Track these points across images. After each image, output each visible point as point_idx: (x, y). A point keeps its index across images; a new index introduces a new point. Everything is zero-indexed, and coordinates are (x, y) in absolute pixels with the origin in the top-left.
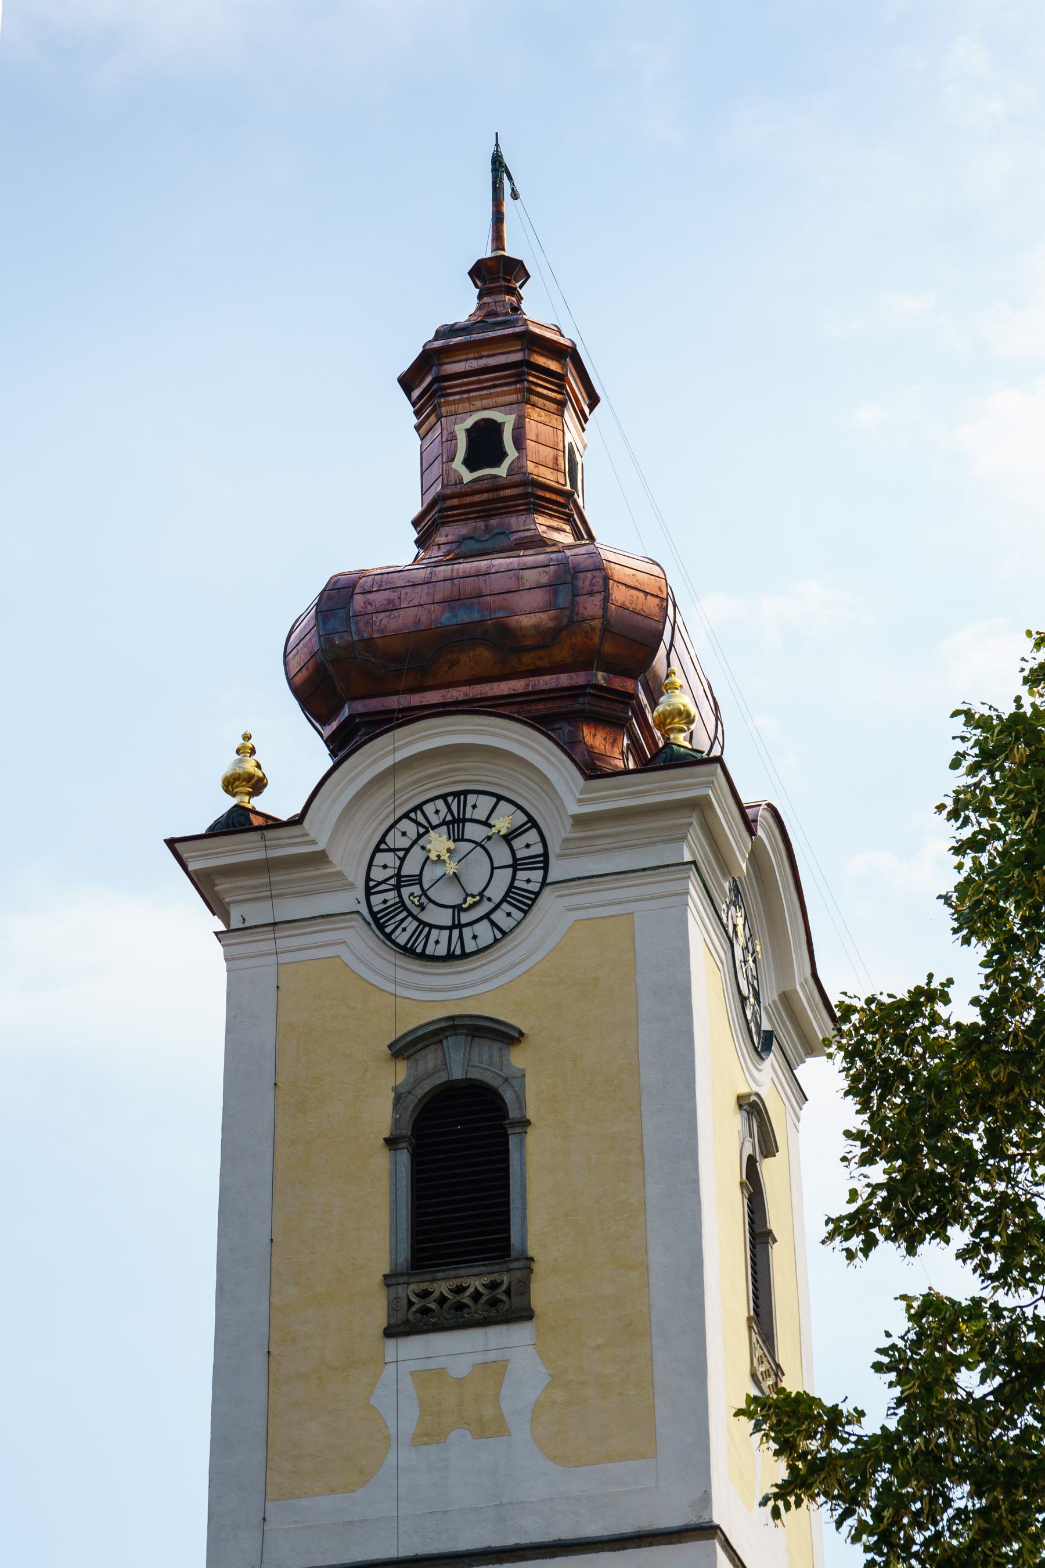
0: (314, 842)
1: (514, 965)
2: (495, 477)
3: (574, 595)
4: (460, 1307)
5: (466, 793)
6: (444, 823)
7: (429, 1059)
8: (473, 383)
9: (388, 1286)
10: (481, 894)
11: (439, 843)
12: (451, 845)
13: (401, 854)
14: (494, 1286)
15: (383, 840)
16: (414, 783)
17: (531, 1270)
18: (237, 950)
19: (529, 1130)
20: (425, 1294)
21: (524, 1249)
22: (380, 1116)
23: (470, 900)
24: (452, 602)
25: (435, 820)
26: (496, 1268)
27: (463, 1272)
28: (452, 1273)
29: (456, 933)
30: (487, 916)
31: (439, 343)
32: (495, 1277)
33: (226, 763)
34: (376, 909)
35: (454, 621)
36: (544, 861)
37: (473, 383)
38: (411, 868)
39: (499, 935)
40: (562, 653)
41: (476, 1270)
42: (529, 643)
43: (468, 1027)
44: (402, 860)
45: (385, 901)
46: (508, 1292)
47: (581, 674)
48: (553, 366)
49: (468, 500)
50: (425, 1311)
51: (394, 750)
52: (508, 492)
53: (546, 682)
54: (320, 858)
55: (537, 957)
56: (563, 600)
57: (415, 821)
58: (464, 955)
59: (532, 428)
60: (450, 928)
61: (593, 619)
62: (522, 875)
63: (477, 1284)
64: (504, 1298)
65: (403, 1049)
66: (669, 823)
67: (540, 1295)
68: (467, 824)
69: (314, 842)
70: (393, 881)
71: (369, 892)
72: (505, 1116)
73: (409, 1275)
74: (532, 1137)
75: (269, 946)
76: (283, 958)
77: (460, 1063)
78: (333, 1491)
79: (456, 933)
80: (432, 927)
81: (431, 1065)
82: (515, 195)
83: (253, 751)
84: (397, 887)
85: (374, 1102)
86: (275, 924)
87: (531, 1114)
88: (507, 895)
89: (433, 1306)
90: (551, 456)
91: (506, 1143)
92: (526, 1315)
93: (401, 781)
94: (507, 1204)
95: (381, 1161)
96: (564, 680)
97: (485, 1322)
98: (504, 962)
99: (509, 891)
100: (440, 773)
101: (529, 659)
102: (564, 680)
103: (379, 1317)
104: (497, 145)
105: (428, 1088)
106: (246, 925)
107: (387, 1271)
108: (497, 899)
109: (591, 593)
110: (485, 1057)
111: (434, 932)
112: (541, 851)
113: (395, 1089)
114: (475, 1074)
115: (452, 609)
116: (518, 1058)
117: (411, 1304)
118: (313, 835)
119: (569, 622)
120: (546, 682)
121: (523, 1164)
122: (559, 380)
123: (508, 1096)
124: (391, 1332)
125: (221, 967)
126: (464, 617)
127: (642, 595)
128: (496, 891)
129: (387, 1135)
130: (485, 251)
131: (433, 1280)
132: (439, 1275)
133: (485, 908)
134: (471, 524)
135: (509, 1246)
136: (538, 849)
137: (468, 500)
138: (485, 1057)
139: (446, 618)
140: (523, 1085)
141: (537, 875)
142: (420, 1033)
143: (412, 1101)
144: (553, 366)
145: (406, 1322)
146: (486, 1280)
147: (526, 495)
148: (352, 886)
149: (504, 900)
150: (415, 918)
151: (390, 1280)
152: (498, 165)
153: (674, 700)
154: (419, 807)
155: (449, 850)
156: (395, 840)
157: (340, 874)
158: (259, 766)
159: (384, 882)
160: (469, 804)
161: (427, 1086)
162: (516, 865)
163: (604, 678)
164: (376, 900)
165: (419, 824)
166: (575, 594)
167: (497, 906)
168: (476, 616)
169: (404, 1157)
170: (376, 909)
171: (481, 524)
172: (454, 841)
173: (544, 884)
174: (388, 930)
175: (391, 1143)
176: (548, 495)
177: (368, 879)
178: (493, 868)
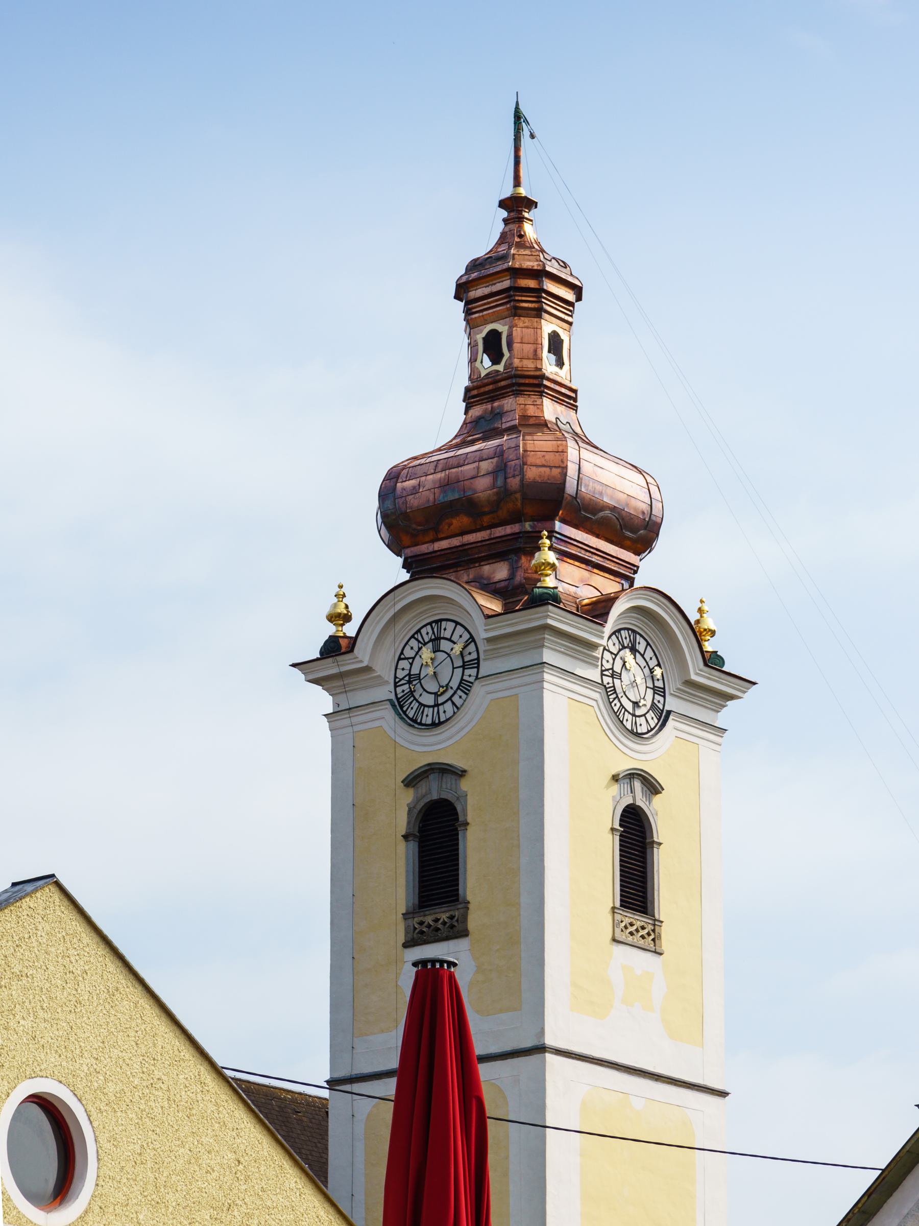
0: (361, 661)
1: (462, 729)
2: (498, 371)
3: (506, 478)
4: (437, 929)
5: (441, 620)
6: (431, 640)
7: (423, 787)
8: (485, 304)
9: (405, 919)
10: (447, 685)
11: (427, 653)
12: (433, 655)
13: (411, 661)
14: (452, 917)
15: (402, 653)
16: (414, 617)
17: (468, 908)
18: (338, 724)
19: (468, 827)
20: (421, 923)
21: (465, 897)
22: (402, 822)
23: (442, 690)
24: (445, 485)
25: (426, 640)
26: (452, 908)
27: (437, 910)
28: (432, 911)
29: (436, 709)
30: (450, 699)
31: (474, 275)
32: (452, 913)
33: (327, 604)
34: (399, 696)
35: (446, 499)
36: (477, 663)
37: (485, 304)
38: (415, 671)
39: (456, 710)
40: (503, 513)
41: (443, 909)
42: (486, 510)
43: (439, 769)
44: (411, 664)
45: (403, 691)
46: (457, 921)
47: (517, 525)
48: (532, 283)
49: (482, 390)
50: (422, 932)
51: (394, 604)
52: (503, 383)
53: (499, 532)
54: (368, 669)
55: (473, 724)
56: (500, 482)
57: (417, 640)
58: (440, 723)
59: (517, 332)
60: (433, 707)
61: (515, 492)
62: (467, 672)
63: (444, 917)
64: (456, 924)
65: (411, 781)
66: (533, 638)
67: (472, 923)
68: (442, 641)
69: (361, 661)
70: (407, 678)
71: (396, 686)
72: (457, 819)
73: (413, 913)
74: (470, 830)
75: (347, 722)
76: (356, 728)
77: (434, 790)
78: (382, 1031)
79: (436, 709)
80: (425, 706)
81: (424, 791)
82: (532, 136)
83: (344, 596)
84: (409, 682)
85: (396, 812)
86: (350, 709)
87: (469, 820)
88: (460, 685)
89: (424, 929)
90: (532, 350)
91: (458, 834)
92: (464, 934)
93: (399, 626)
94: (458, 870)
95: (402, 846)
96: (509, 530)
97: (447, 938)
98: (454, 730)
99: (461, 682)
100: (425, 611)
101: (486, 520)
102: (509, 530)
103: (401, 939)
104: (517, 103)
105: (422, 804)
106: (340, 709)
107: (404, 912)
108: (455, 688)
109: (514, 476)
110: (449, 785)
111: (426, 709)
112: (476, 657)
113: (408, 805)
114: (444, 796)
115: (445, 492)
116: (465, 785)
117: (415, 929)
118: (360, 658)
119: (504, 494)
120: (499, 532)
121: (465, 847)
122: (539, 292)
123: (459, 808)
124: (406, 945)
125: (319, 741)
126: (452, 496)
127: (548, 469)
128: (455, 684)
129: (403, 833)
130: (507, 192)
131: (425, 916)
132: (427, 913)
133: (450, 692)
134: (484, 407)
135: (458, 895)
136: (474, 656)
137: (482, 390)
138: (449, 785)
139: (441, 499)
140: (466, 801)
141: (473, 672)
142: (416, 773)
143: (416, 811)
144: (532, 283)
145: (413, 939)
146: (448, 915)
147: (513, 385)
148: (387, 682)
149: (458, 688)
150: (417, 701)
151: (406, 916)
152: (518, 117)
153: (544, 557)
154: (419, 631)
155: (432, 659)
156: (408, 653)
157: (379, 676)
158: (347, 607)
159: (403, 679)
160: (443, 627)
161: (422, 804)
162: (464, 667)
163: (531, 526)
164: (399, 690)
165: (419, 642)
166: (506, 478)
167: (455, 693)
168: (457, 496)
169: (413, 846)
170: (399, 696)
171: (489, 406)
172: (434, 652)
173: (477, 678)
174: (405, 709)
175: (406, 837)
176: (527, 381)
177: (396, 677)
178: (454, 668)
